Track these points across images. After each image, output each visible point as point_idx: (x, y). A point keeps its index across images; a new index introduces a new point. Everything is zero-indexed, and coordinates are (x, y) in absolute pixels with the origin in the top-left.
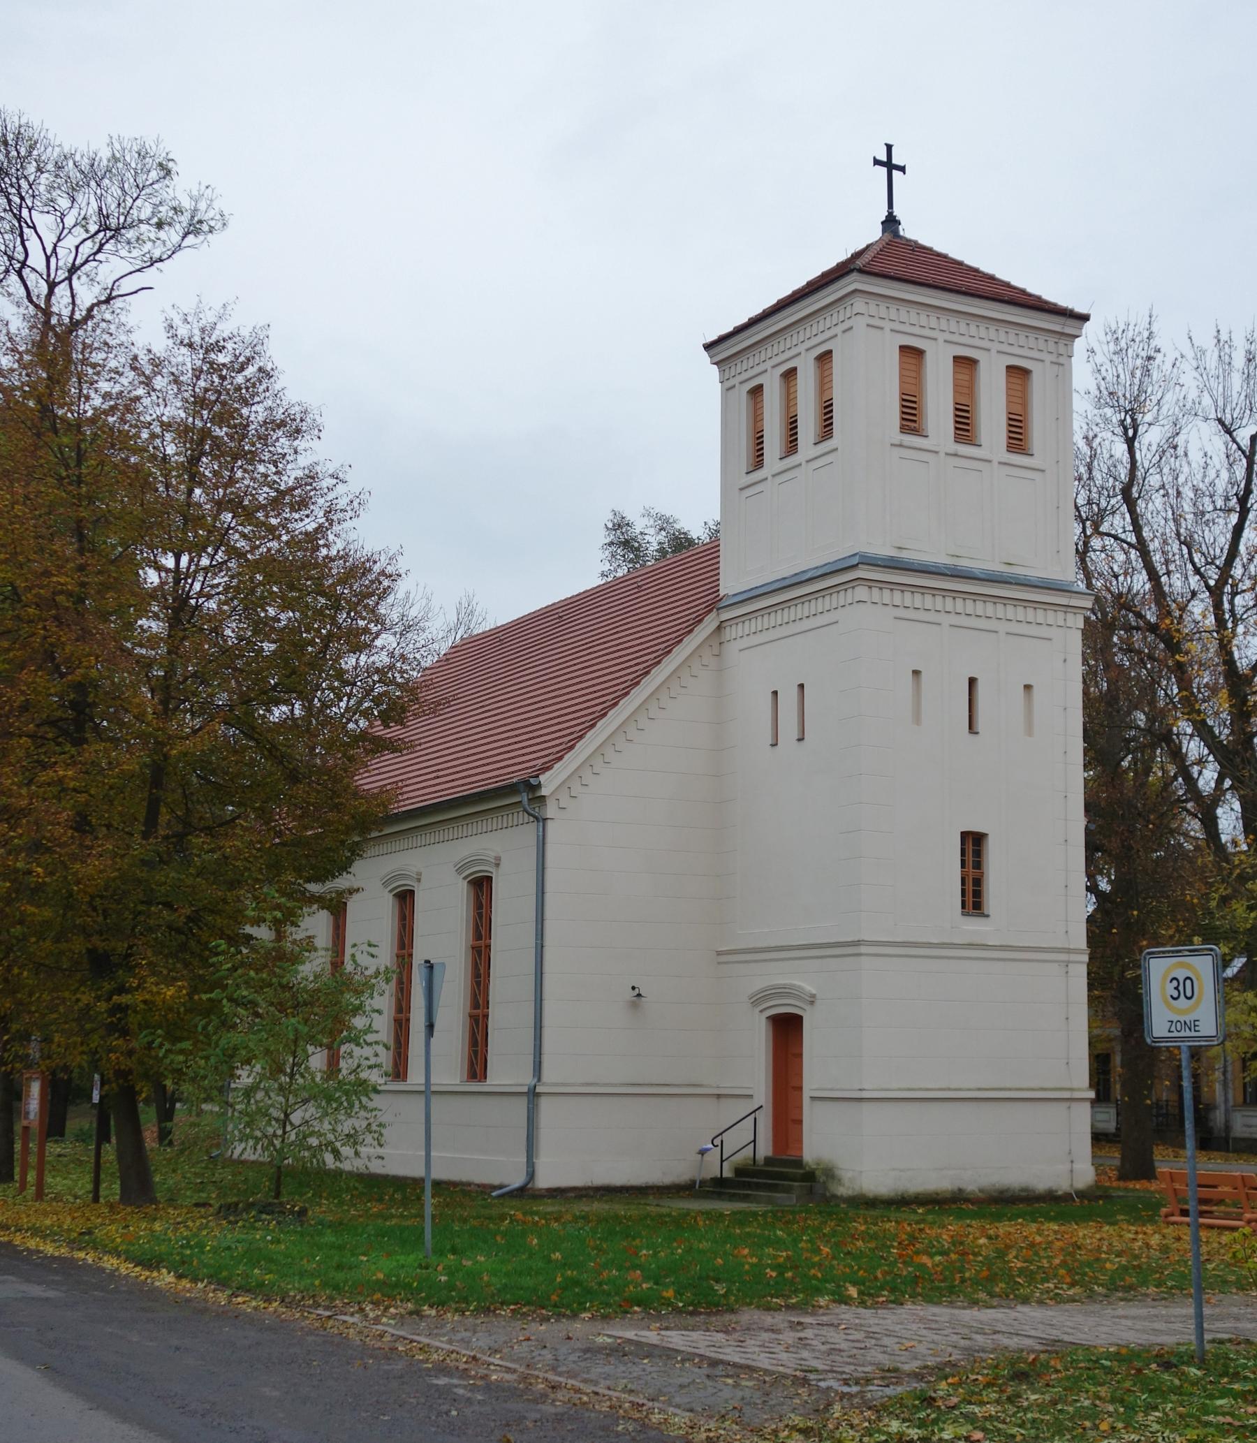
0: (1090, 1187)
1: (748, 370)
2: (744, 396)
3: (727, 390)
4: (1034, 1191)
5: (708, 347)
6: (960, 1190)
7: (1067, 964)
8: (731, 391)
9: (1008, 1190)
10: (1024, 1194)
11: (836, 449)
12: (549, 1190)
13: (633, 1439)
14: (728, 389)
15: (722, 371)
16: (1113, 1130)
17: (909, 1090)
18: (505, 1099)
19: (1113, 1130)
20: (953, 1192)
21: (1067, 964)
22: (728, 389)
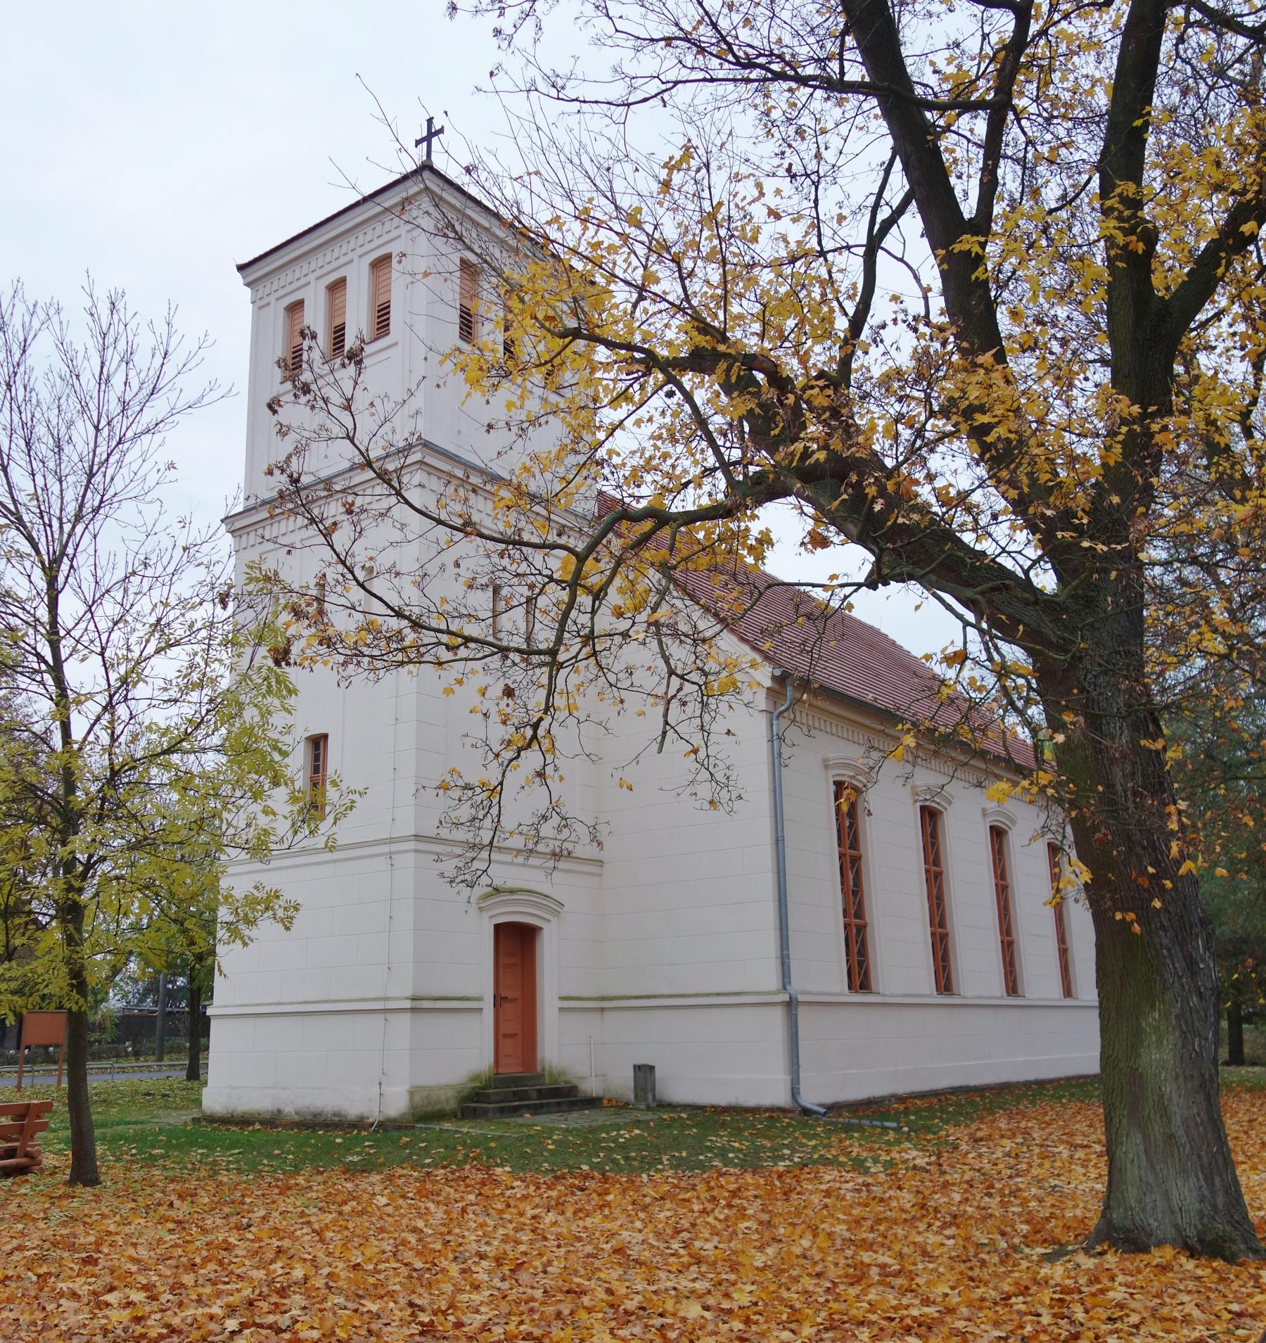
0: (403, 1115)
1: (286, 287)
2: (281, 314)
3: (259, 305)
4: (345, 1116)
5: (241, 268)
6: (279, 1111)
7: (390, 855)
8: (263, 311)
9: (320, 1114)
10: (336, 1119)
11: (396, 343)
12: (834, 1108)
13: (740, 1339)
14: (260, 308)
15: (255, 291)
16: (1094, 1068)
17: (279, 1004)
18: (359, 1017)
19: (1094, 1068)
20: (273, 1113)
21: (390, 855)
22: (260, 308)
